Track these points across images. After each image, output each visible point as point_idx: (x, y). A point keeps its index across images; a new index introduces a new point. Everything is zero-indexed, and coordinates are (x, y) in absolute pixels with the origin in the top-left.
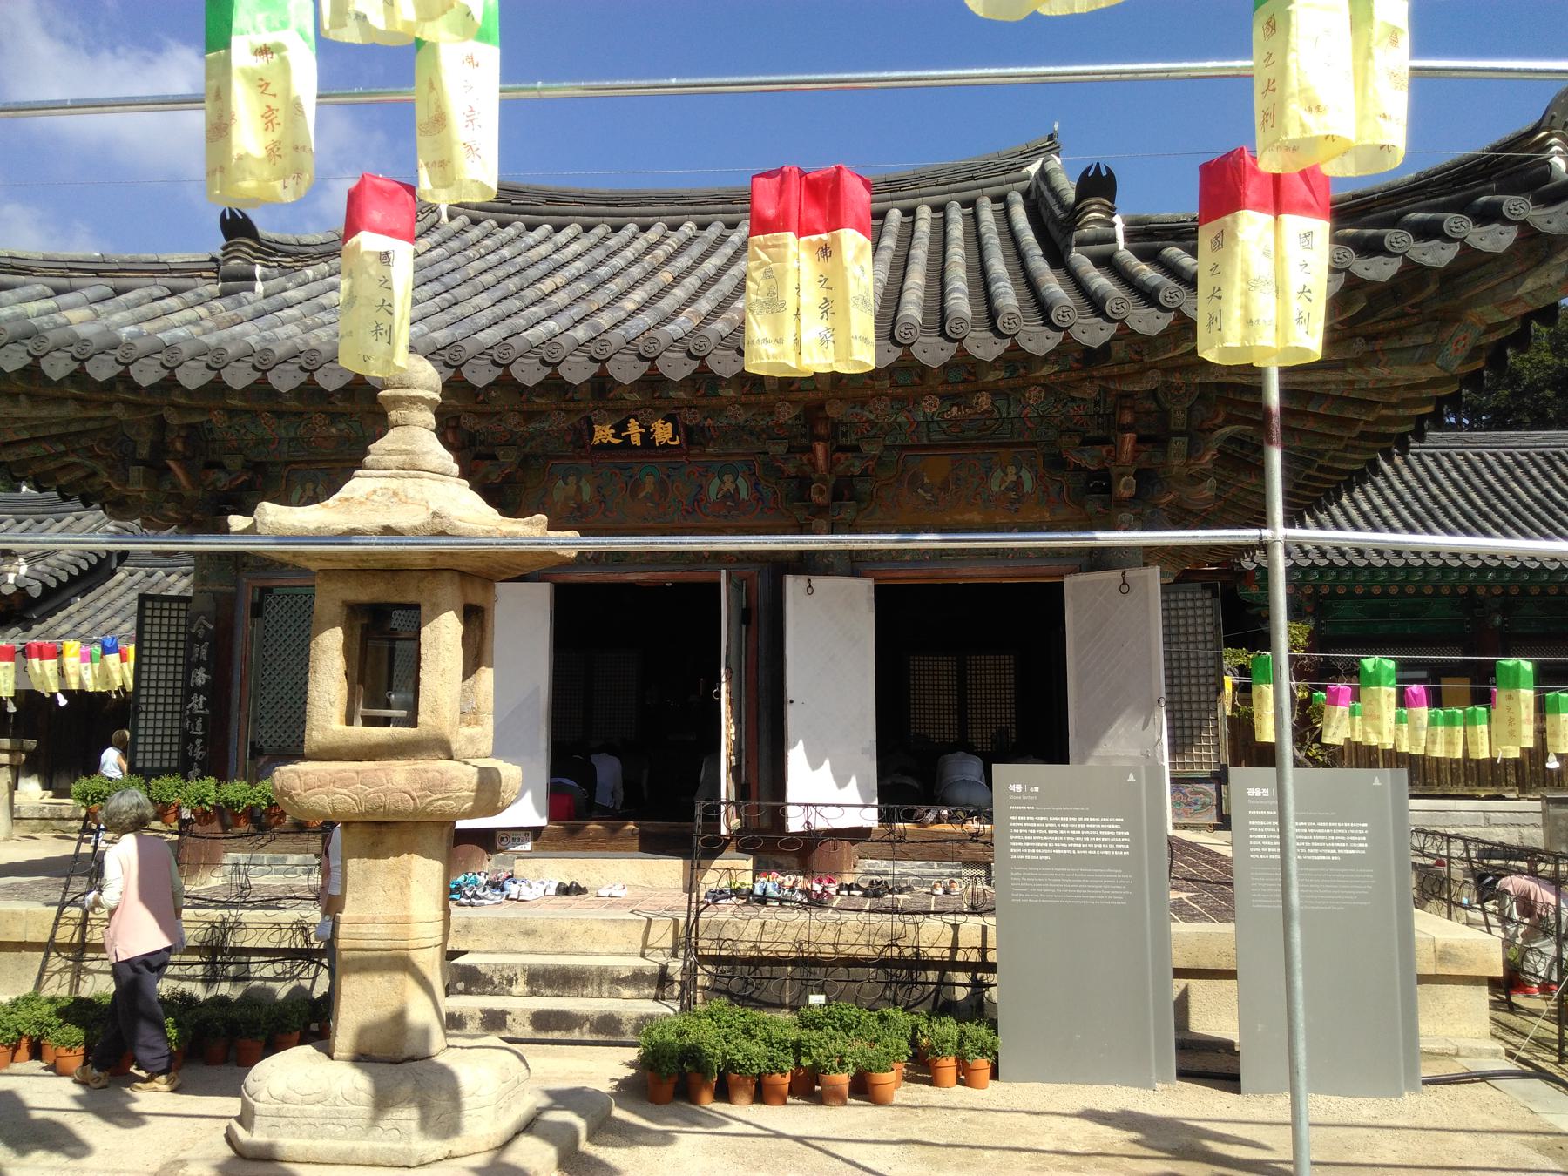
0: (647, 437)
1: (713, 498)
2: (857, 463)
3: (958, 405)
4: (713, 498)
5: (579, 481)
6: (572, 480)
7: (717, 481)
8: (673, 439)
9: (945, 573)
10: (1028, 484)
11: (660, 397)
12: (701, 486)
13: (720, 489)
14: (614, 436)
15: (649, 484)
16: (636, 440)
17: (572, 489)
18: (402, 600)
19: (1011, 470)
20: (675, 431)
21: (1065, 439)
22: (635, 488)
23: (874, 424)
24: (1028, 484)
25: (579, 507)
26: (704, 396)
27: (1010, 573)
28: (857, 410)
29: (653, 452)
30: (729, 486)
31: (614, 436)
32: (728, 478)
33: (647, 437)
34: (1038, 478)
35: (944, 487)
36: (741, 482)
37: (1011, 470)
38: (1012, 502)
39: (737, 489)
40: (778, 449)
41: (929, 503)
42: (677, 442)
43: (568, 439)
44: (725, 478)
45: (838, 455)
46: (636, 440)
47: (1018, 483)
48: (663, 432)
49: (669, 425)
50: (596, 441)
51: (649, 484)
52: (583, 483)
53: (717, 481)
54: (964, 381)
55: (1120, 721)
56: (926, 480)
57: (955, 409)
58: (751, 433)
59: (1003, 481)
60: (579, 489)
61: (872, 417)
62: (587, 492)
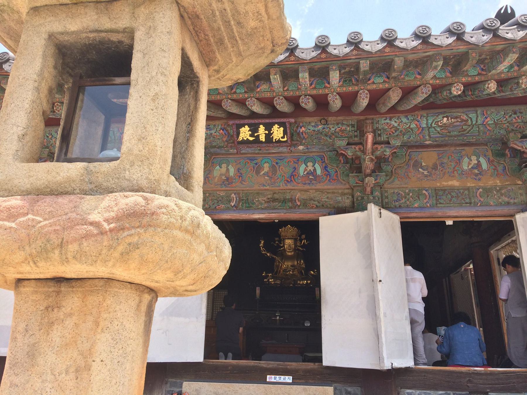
0: (269, 136)
1: (302, 174)
2: (388, 150)
3: (447, 117)
4: (302, 174)
5: (228, 166)
6: (224, 166)
7: (303, 166)
8: (283, 138)
9: (440, 214)
10: (484, 165)
11: (288, 90)
12: (295, 168)
13: (305, 170)
14: (251, 136)
15: (266, 167)
16: (262, 138)
17: (224, 170)
18: (113, 27)
19: (474, 158)
20: (285, 132)
21: (512, 135)
22: (258, 169)
23: (397, 129)
24: (484, 165)
25: (228, 179)
26: (315, 88)
27: (480, 214)
28: (388, 121)
29: (271, 145)
30: (310, 168)
31: (251, 136)
32: (310, 164)
33: (269, 136)
34: (489, 162)
35: (435, 167)
36: (317, 166)
37: (474, 158)
38: (476, 175)
39: (315, 170)
40: (341, 143)
41: (426, 176)
42: (285, 139)
43: (225, 139)
44: (309, 164)
45: (376, 146)
46: (262, 138)
47: (479, 165)
48: (278, 133)
49: (282, 129)
50: (240, 139)
51: (266, 167)
52: (230, 167)
53: (303, 166)
54: (479, 74)
55: (385, 368)
56: (423, 164)
57: (445, 119)
58: (326, 136)
59: (469, 164)
60: (228, 170)
61: (396, 125)
62: (232, 171)
